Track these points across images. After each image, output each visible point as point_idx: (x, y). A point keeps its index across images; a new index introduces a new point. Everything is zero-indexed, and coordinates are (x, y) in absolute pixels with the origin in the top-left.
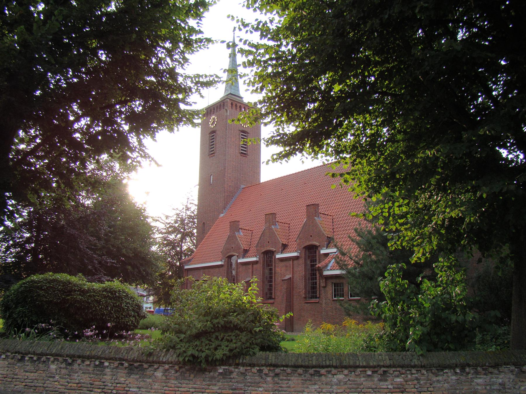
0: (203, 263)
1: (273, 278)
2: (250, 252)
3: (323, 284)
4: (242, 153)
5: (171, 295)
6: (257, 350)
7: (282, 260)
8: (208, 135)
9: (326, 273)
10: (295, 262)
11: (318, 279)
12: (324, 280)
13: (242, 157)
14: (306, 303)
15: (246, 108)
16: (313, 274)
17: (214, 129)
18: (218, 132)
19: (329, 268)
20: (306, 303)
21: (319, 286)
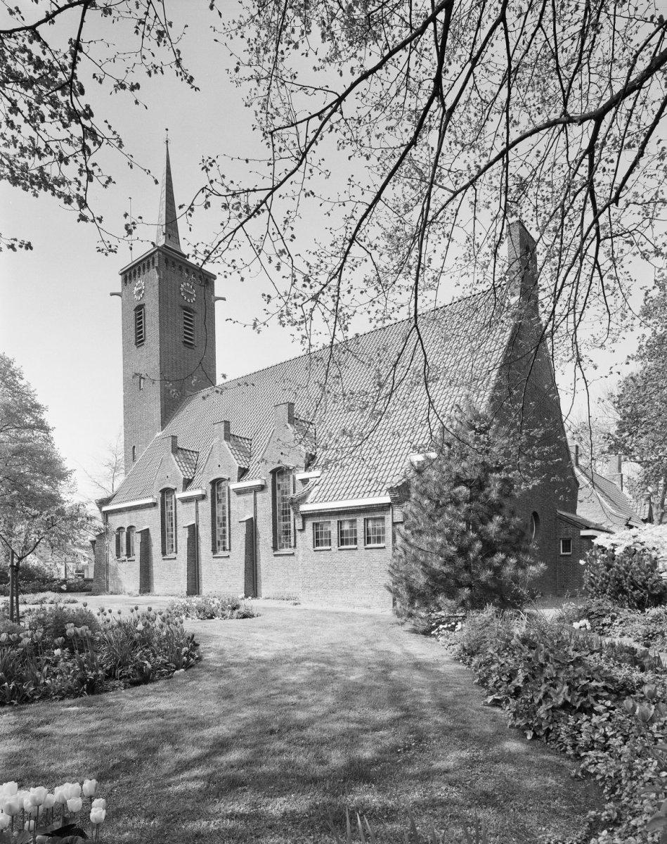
0: (356, 495)
1: (227, 519)
2: (194, 482)
3: (299, 526)
4: (185, 342)
5: (619, 403)
6: (309, 450)
7: (239, 492)
8: (134, 313)
9: (304, 508)
10: (259, 495)
11: (292, 519)
12: (301, 520)
13: (186, 349)
14: (275, 555)
15: (191, 271)
16: (286, 511)
17: (142, 303)
18: (146, 307)
19: (308, 500)
20: (275, 555)
21: (295, 530)
